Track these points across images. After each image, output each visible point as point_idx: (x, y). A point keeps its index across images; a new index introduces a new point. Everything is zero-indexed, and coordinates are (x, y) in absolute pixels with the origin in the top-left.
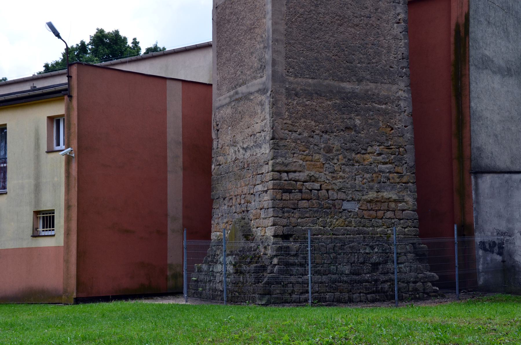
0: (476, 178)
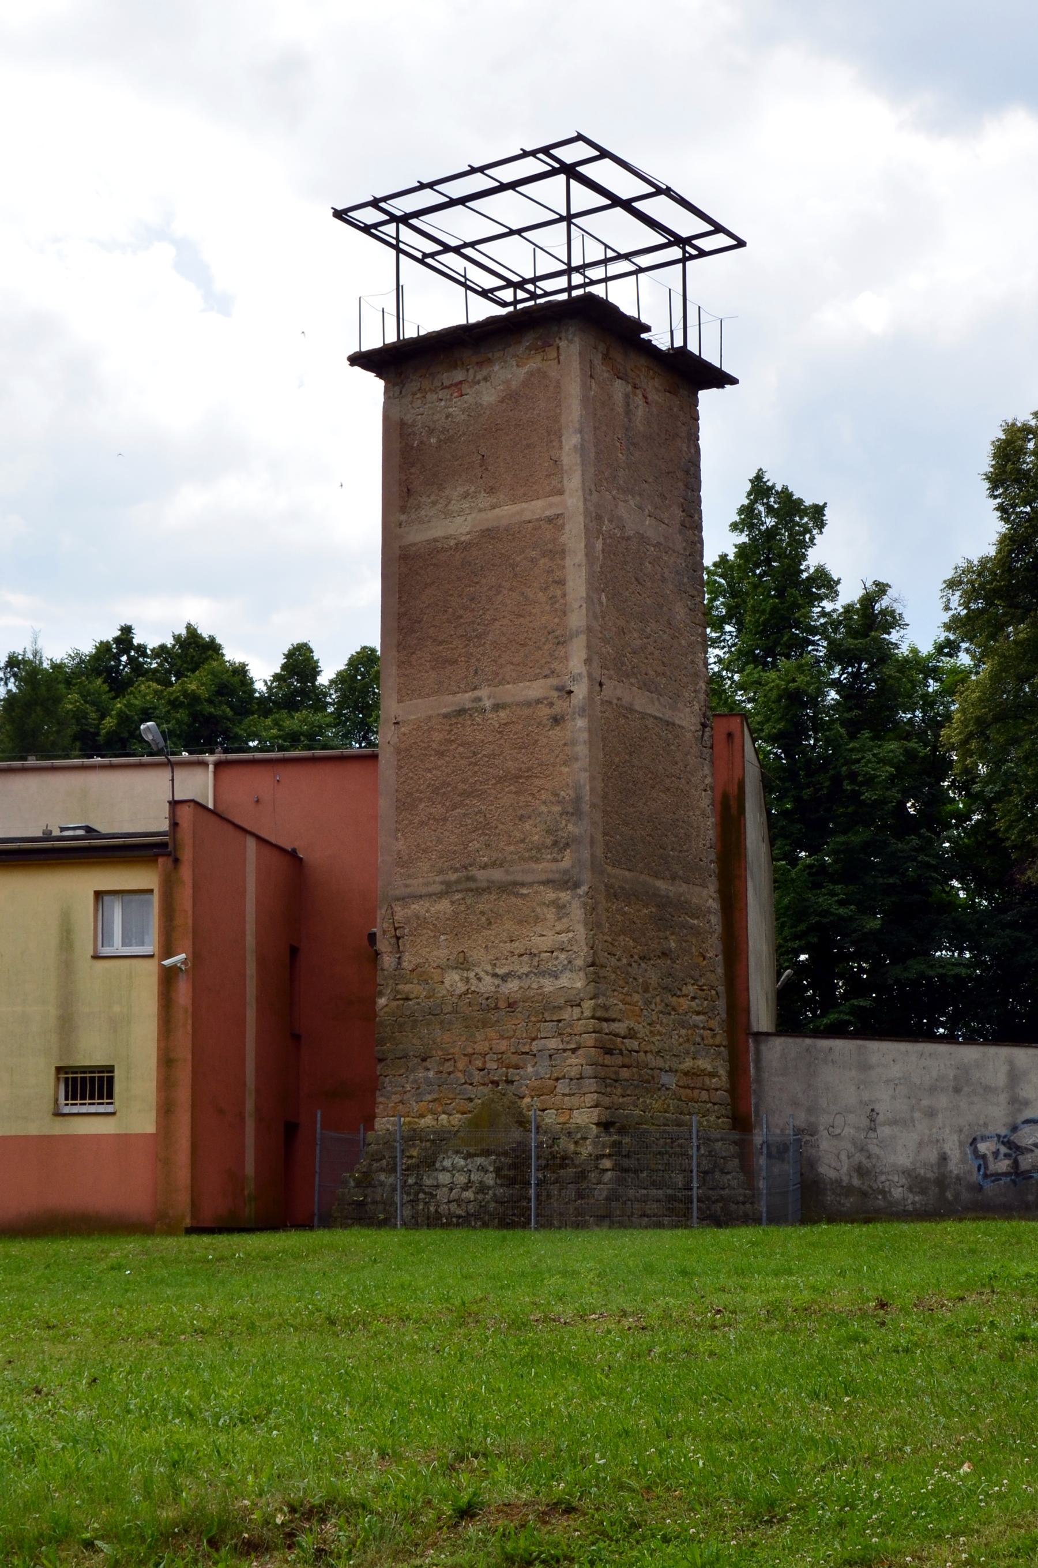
0: (757, 1043)
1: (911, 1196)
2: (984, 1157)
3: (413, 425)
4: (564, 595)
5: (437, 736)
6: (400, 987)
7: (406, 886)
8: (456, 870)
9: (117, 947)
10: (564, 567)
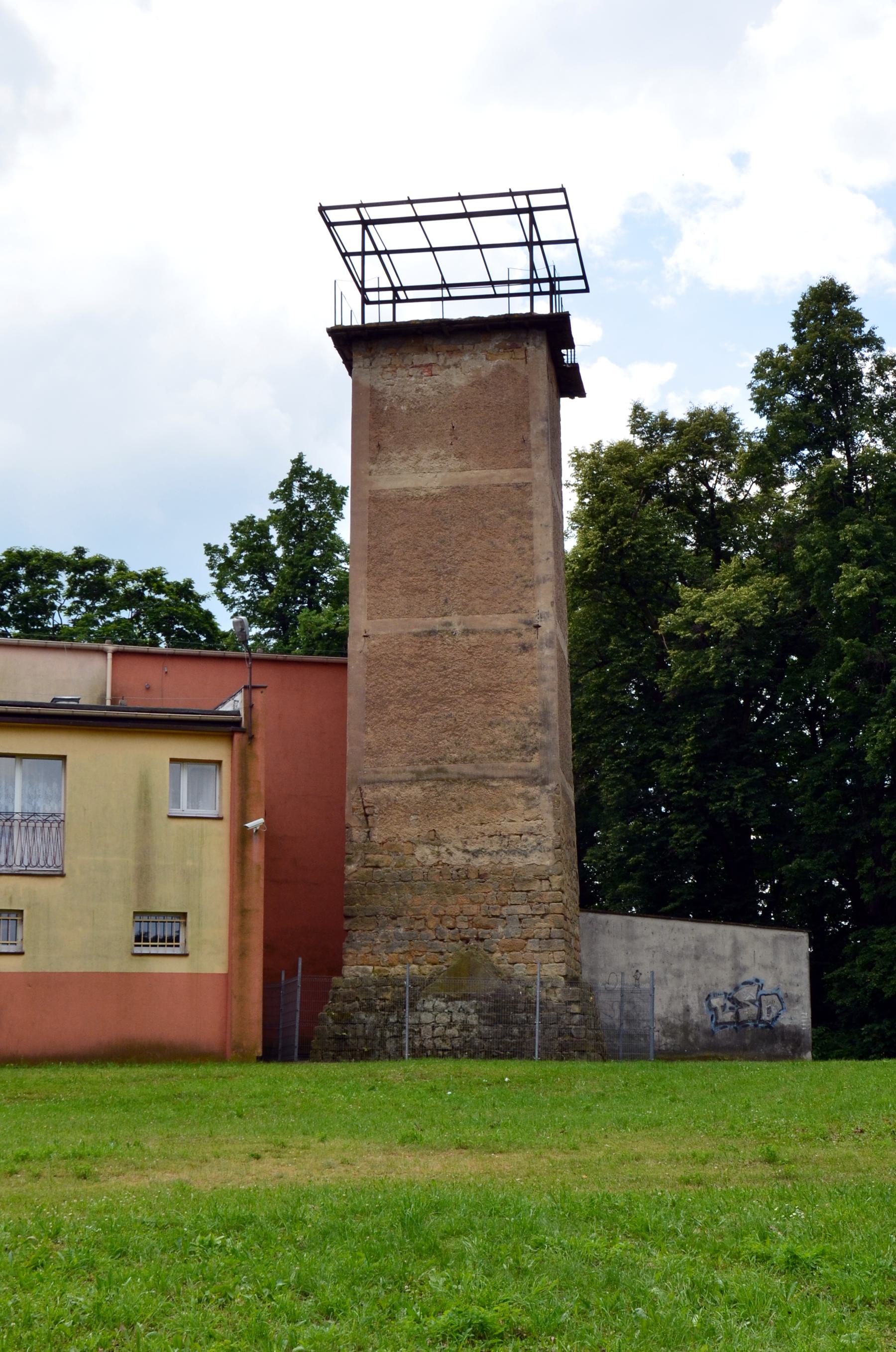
1: (664, 1038)
2: (715, 1009)
3: (383, 392)
4: (532, 548)
5: (407, 650)
6: (369, 856)
7: (376, 772)
8: (427, 762)
9: (185, 809)
10: (531, 526)
